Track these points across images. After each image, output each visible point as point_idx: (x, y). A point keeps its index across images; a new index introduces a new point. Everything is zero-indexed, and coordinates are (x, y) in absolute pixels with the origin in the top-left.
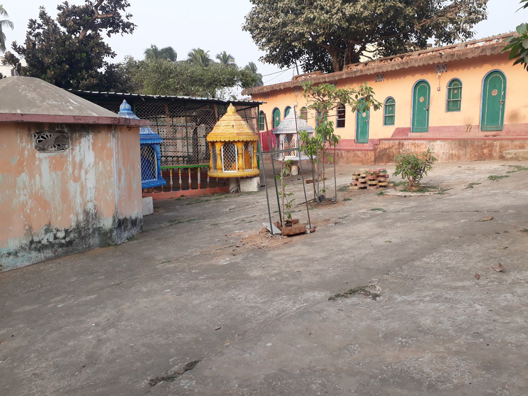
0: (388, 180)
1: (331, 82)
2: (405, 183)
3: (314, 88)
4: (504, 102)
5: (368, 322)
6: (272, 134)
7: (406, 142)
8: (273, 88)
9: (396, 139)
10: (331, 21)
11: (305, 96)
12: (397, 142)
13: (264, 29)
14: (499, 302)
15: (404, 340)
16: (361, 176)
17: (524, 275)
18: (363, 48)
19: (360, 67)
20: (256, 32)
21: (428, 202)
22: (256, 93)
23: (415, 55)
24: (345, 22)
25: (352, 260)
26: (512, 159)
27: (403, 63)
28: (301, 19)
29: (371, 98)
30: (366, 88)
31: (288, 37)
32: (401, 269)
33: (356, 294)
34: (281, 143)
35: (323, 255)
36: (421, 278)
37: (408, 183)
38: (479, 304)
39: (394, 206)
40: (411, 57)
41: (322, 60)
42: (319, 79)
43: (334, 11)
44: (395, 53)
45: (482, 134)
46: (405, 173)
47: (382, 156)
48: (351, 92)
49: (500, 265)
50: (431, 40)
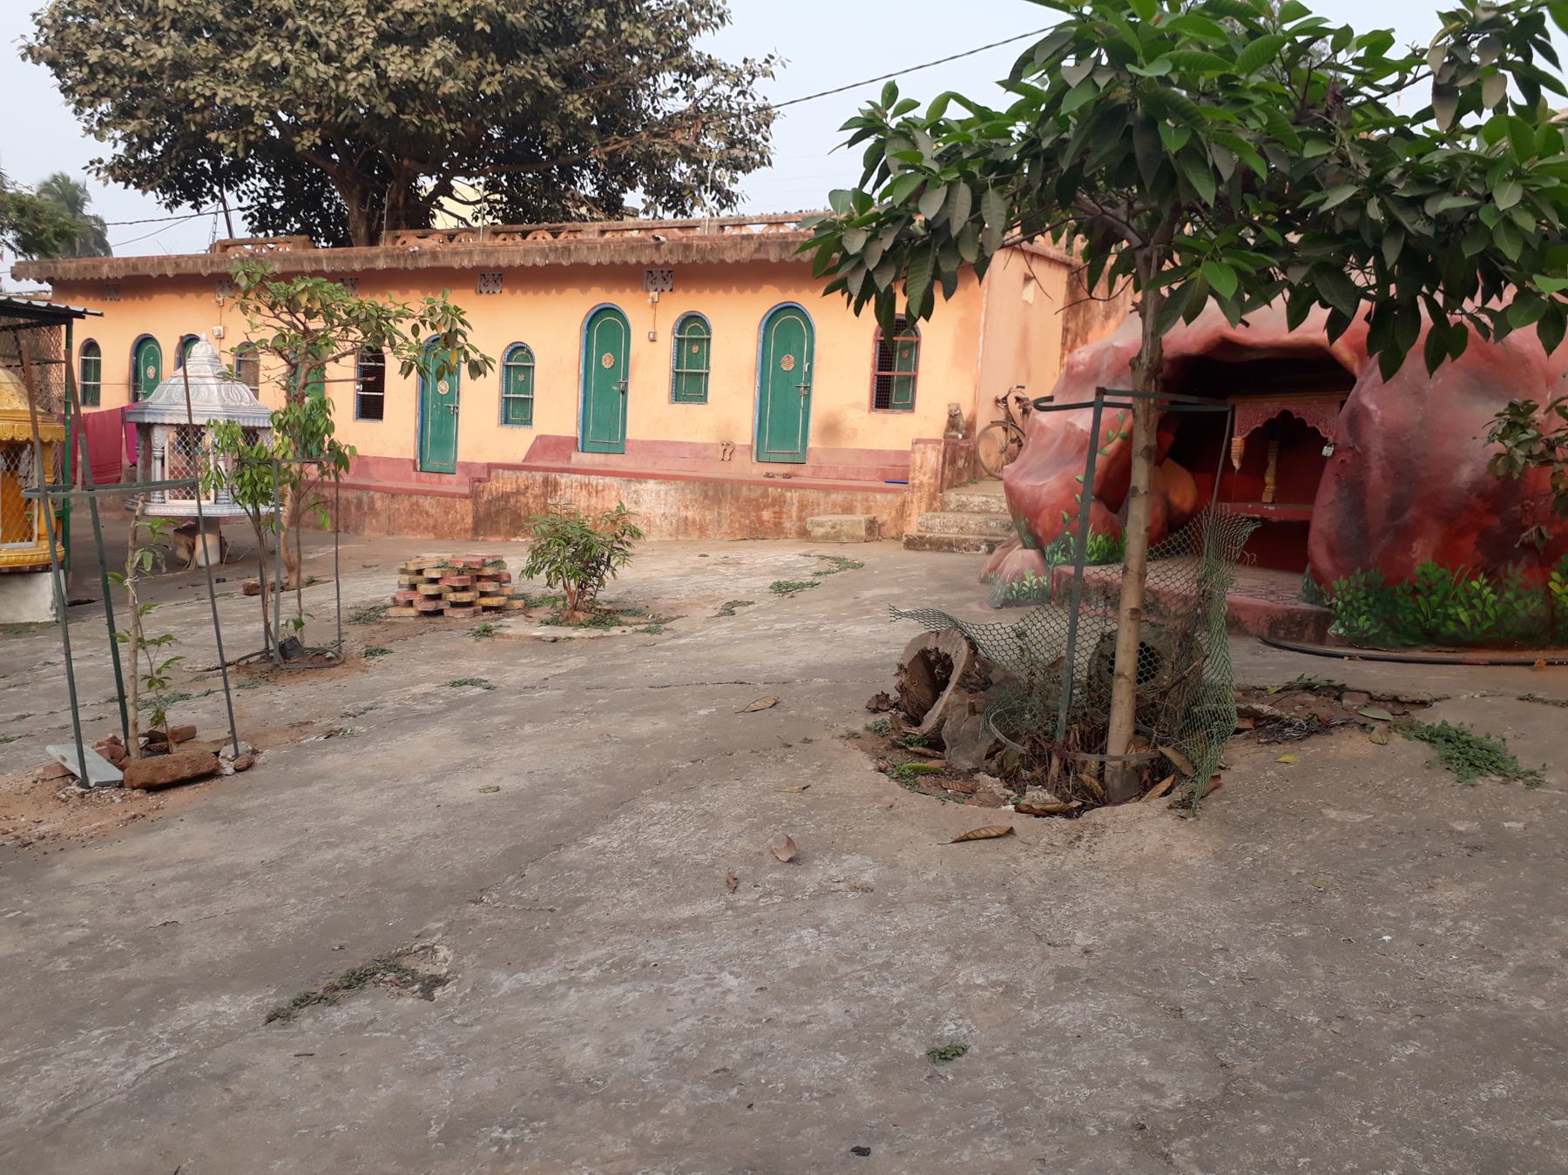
0: (507, 591)
1: (333, 277)
2: (556, 599)
3: (273, 287)
4: (808, 388)
5: (399, 1086)
6: (123, 421)
7: (564, 479)
8: (135, 267)
9: (538, 469)
10: (342, 89)
11: (244, 309)
12: (539, 476)
13: (108, 72)
14: (784, 960)
15: (508, 1135)
16: (427, 575)
17: (846, 865)
18: (445, 189)
19: (430, 243)
20: (76, 73)
21: (616, 656)
22: (72, 276)
23: (590, 232)
24: (387, 100)
25: (368, 863)
26: (826, 538)
27: (557, 249)
28: (240, 63)
29: (460, 338)
30: (445, 309)
31: (195, 111)
32: (518, 882)
33: (369, 985)
34: (158, 454)
35: (270, 852)
36: (578, 903)
37: (565, 598)
38: (731, 973)
39: (519, 670)
40: (579, 236)
41: (313, 202)
42: (299, 261)
43: (352, 59)
44: (536, 216)
45: (758, 471)
46: (558, 570)
47: (497, 516)
48: (399, 314)
49: (790, 842)
50: (634, 198)
